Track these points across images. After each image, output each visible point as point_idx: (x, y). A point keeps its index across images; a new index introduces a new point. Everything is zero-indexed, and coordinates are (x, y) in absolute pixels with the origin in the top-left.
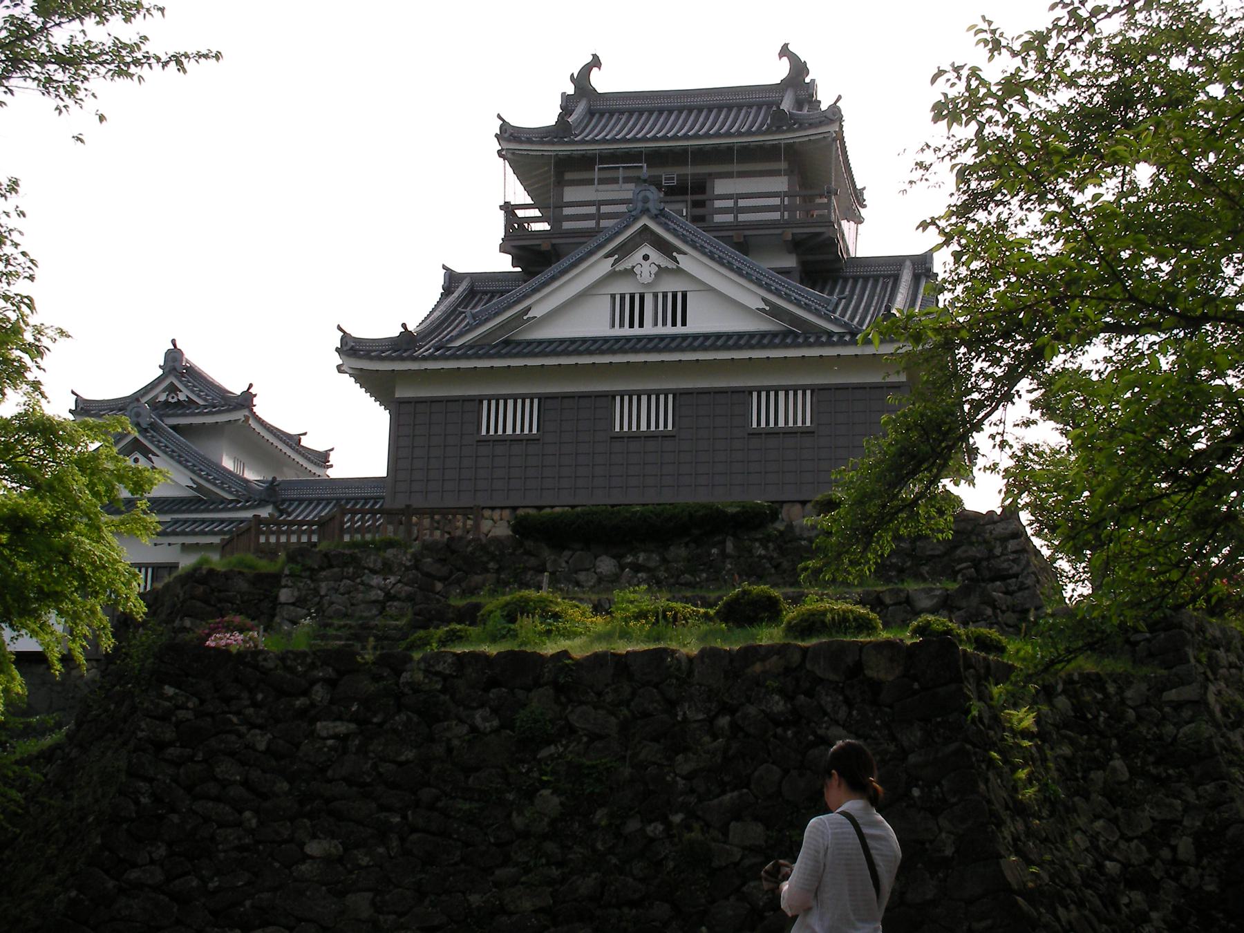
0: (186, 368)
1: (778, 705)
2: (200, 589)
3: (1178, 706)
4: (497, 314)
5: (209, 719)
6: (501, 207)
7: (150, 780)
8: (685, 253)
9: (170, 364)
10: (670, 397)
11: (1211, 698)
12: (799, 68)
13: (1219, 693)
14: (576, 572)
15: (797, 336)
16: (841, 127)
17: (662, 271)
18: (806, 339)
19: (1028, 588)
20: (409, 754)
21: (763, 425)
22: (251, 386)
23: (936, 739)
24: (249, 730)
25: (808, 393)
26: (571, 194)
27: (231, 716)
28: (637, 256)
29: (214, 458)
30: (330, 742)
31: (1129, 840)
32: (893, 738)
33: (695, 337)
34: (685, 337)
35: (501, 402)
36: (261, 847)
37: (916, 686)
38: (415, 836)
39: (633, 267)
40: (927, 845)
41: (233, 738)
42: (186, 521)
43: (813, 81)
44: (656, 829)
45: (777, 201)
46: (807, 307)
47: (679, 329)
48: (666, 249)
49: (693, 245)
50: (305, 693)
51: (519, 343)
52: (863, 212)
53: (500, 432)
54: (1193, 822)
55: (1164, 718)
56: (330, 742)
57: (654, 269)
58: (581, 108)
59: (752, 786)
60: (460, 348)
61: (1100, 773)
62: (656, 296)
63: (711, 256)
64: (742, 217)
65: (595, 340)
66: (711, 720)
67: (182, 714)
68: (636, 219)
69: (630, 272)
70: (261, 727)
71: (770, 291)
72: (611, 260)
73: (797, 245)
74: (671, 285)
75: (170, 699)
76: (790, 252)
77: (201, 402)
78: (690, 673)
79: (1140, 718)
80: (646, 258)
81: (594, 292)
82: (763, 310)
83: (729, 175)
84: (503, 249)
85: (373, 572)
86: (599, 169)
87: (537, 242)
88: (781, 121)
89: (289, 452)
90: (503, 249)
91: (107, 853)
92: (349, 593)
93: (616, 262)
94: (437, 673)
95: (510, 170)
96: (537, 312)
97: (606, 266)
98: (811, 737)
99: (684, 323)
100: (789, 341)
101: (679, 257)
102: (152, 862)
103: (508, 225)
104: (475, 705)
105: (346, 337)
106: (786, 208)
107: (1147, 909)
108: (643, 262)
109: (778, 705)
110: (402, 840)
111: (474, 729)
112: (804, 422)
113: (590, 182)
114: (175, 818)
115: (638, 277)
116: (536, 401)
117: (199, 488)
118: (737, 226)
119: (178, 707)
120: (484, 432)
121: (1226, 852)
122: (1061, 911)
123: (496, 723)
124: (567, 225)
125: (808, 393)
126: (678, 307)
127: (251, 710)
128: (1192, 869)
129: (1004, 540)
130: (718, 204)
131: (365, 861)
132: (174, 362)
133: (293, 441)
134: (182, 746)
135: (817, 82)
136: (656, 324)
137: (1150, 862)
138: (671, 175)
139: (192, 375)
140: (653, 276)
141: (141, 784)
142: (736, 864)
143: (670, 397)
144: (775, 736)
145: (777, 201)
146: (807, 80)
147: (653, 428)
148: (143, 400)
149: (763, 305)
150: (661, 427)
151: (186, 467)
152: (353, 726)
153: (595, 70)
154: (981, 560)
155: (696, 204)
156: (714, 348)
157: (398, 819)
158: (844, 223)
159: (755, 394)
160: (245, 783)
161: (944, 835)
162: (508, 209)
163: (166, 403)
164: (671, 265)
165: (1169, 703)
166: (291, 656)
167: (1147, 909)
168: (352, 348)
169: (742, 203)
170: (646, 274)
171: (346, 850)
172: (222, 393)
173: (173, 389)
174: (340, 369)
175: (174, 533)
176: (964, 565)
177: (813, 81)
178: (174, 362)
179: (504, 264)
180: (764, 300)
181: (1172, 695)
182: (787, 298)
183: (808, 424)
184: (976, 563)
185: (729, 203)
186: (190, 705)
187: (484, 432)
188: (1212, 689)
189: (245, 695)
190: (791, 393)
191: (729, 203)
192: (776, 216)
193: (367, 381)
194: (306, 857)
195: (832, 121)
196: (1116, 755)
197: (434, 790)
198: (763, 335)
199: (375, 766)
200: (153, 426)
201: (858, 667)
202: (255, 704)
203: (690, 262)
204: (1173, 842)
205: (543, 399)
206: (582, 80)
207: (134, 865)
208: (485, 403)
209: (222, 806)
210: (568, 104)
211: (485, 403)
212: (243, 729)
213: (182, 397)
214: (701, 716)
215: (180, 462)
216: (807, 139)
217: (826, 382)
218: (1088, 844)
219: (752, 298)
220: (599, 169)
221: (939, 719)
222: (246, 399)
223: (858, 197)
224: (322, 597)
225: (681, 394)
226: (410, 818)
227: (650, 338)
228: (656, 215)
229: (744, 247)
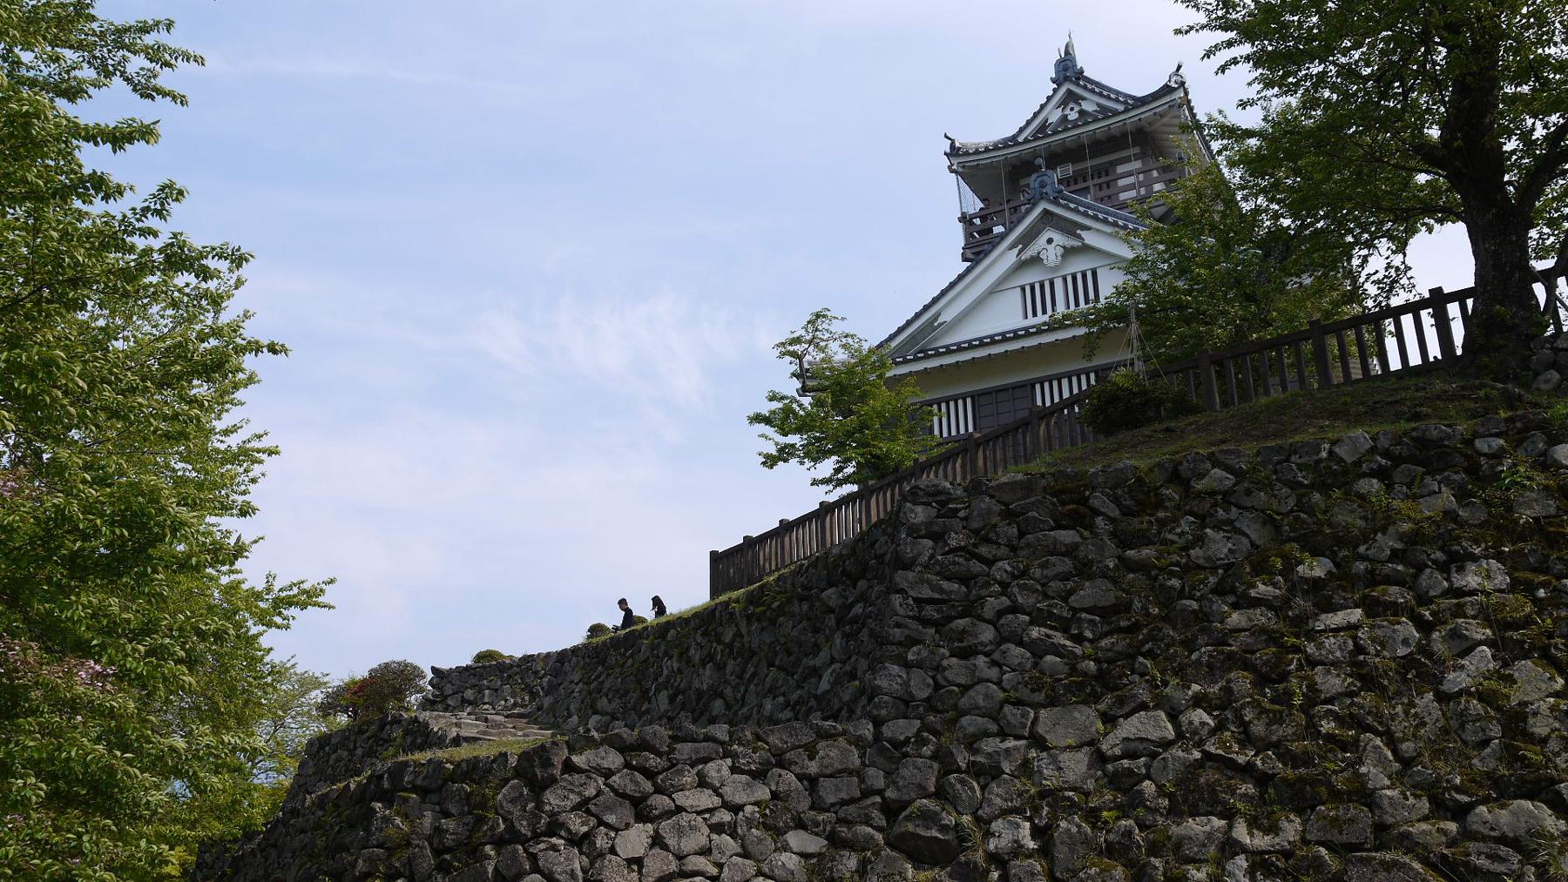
8: (1089, 229)
10: (969, 401)
17: (1068, 252)
28: (1042, 240)
35: (1055, 383)
39: (1039, 253)
48: (1070, 228)
57: (1060, 251)
68: (1034, 205)
69: (1036, 260)
72: (1016, 251)
80: (1050, 241)
93: (1020, 252)
96: (947, 317)
97: (1011, 258)
101: (1084, 234)
106: (1141, 185)
108: (1048, 247)
132: (1068, 71)
140: (1059, 258)
143: (969, 401)
164: (1076, 243)
170: (1052, 258)
205: (975, 396)
216: (1152, 113)
217: (1108, 361)
225: (979, 395)
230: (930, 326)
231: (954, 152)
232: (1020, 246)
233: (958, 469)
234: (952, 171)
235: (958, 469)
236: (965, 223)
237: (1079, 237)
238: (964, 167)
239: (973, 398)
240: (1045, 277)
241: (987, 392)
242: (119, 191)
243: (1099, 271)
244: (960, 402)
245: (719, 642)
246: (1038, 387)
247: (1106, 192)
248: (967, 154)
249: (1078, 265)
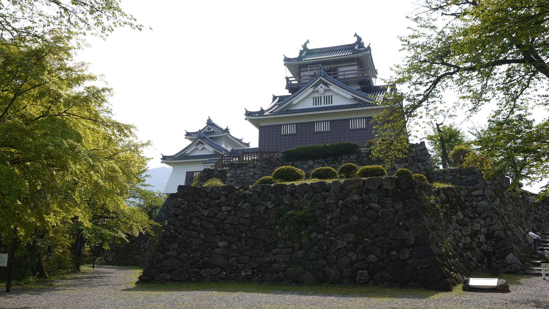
0: (212, 123)
1: (357, 198)
2: (206, 174)
3: (477, 196)
4: (284, 104)
5: (191, 207)
6: (285, 78)
7: (174, 225)
9: (208, 123)
11: (486, 194)
12: (359, 39)
13: (488, 192)
14: (302, 165)
15: (361, 105)
16: (371, 51)
17: (325, 90)
18: (363, 105)
19: (429, 164)
20: (247, 215)
22: (228, 127)
23: (407, 207)
24: (203, 210)
26: (302, 74)
27: (197, 206)
28: (319, 87)
29: (219, 145)
30: (225, 213)
31: (465, 236)
32: (393, 207)
33: (335, 106)
34: (332, 107)
36: (205, 244)
37: (399, 190)
38: (250, 240)
40: (406, 241)
41: (197, 212)
42: (212, 160)
43: (363, 42)
44: (320, 236)
45: (354, 72)
46: (363, 97)
47: (330, 105)
49: (333, 83)
50: (219, 199)
51: (290, 111)
52: (377, 76)
53: (355, 128)
54: (484, 230)
55: (473, 200)
56: (225, 213)
57: (324, 90)
58: (305, 53)
59: (350, 223)
60: (275, 113)
61: (455, 216)
62: (324, 97)
63: (338, 86)
64: (346, 77)
65: (309, 109)
66: (336, 203)
67: (183, 206)
69: (317, 91)
70: (206, 209)
71: (353, 93)
72: (313, 88)
73: (360, 83)
74: (328, 94)
75: (180, 202)
76: (359, 85)
77: (216, 131)
78: (330, 188)
79: (466, 201)
80: (321, 87)
81: (309, 97)
82: (352, 99)
83: (342, 67)
84: (286, 88)
85: (251, 168)
86: (309, 67)
87: (295, 86)
88: (355, 52)
89: (239, 143)
90: (286, 88)
91: (161, 247)
92: (245, 173)
93: (314, 89)
94: (256, 191)
95: (287, 69)
96: (294, 103)
98: (367, 207)
99: (332, 103)
100: (359, 106)
101: (330, 86)
102: (174, 249)
103: (287, 82)
104: (267, 200)
105: (247, 111)
107: (472, 257)
109: (357, 198)
110: (246, 241)
111: (267, 207)
112: (364, 127)
113: (307, 71)
114: (181, 236)
116: (295, 125)
117: (215, 152)
118: (345, 79)
119: (182, 204)
120: (282, 133)
121: (495, 239)
122: (449, 260)
123: (273, 205)
124: (302, 82)
125: (364, 119)
126: (329, 99)
127: (203, 204)
128: (484, 244)
129: (421, 151)
130: (340, 74)
131: (235, 248)
132: (210, 123)
133: (240, 141)
134: (183, 215)
135: (364, 42)
136: (325, 104)
137: (471, 243)
138: (327, 67)
139: (214, 125)
141: (171, 226)
142: (345, 247)
144: (356, 207)
145: (354, 72)
146: (362, 42)
147: (325, 130)
148: (202, 132)
149: (352, 97)
150: (327, 130)
151: (212, 147)
152: (232, 208)
153: (308, 44)
154: (415, 157)
155: (334, 74)
156: (339, 109)
157: (245, 235)
158: (373, 78)
159: (351, 120)
160: (201, 225)
161: (411, 237)
162: (287, 78)
163: (208, 132)
165: (474, 195)
166: (215, 188)
167: (472, 257)
168: (248, 114)
169: (346, 73)
170: (321, 91)
171: (229, 244)
172: (221, 129)
173: (209, 129)
174: (246, 119)
175: (209, 163)
176: (410, 158)
177: (363, 42)
178: (210, 123)
179: (287, 93)
180: (352, 96)
181: (476, 193)
182: (358, 95)
183: (365, 127)
184: (413, 158)
185: (343, 73)
186: (186, 203)
187: (282, 133)
188: (486, 191)
189: (202, 200)
191: (343, 73)
192: (355, 75)
193: (252, 121)
194: (218, 247)
195: (368, 50)
196: (459, 211)
197: (255, 226)
198: (352, 105)
199: (238, 219)
200: (204, 137)
201: (381, 185)
202: (204, 202)
203: (333, 88)
204: (478, 236)
205: (297, 124)
206: (305, 46)
207: (169, 250)
208: (316, 123)
209: (194, 232)
210: (301, 52)
211: (316, 123)
212: (201, 209)
213: (212, 130)
214: (333, 201)
215: (210, 146)
218: (453, 238)
219: (349, 96)
220: (309, 67)
221: (407, 201)
222: (227, 130)
223: (376, 72)
224: (238, 175)
226: (248, 234)
227: (323, 108)
228: (324, 76)
229: (347, 84)
233: (546, 248)
235: (546, 248)
237: (329, 87)
239: (365, 118)
240: (319, 96)
242: (406, 100)
243: (333, 96)
245: (369, 266)
247: (335, 76)
249: (328, 94)
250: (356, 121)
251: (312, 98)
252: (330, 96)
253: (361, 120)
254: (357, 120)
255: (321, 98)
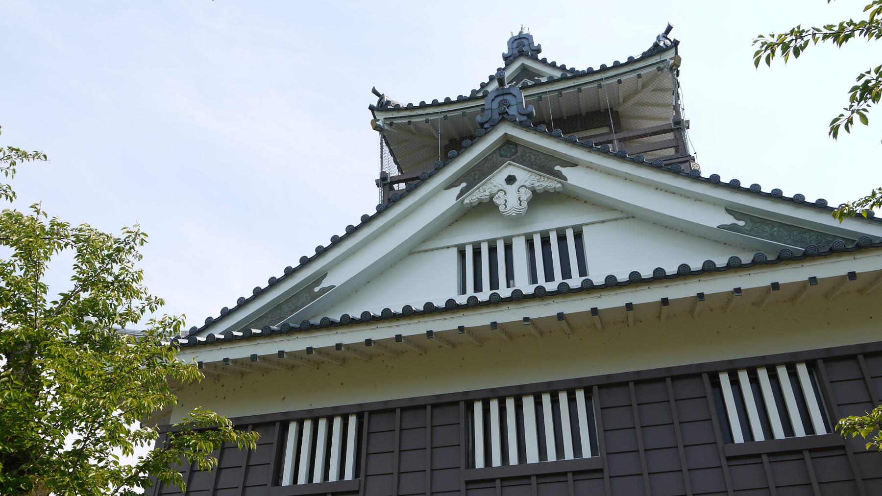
10: (352, 421)
21: (569, 454)
25: (580, 396)
28: (498, 179)
53: (513, 460)
57: (526, 195)
72: (457, 190)
80: (511, 180)
82: (732, 227)
97: (449, 200)
101: (566, 171)
108: (508, 188)
115: (501, 208)
120: (480, 463)
140: (525, 204)
143: (352, 421)
164: (552, 184)
180: (731, 210)
183: (587, 453)
187: (480, 463)
190: (546, 400)
208: (478, 408)
211: (478, 408)
225: (371, 413)
230: (307, 290)
231: (382, 106)
232: (464, 185)
234: (376, 128)
236: (384, 186)
237: (559, 175)
238: (391, 124)
239: (360, 417)
241: (385, 410)
243: (587, 233)
244: (307, 426)
246: (293, 428)
248: (397, 108)
250: (519, 408)
251: (454, 252)
252: (570, 236)
253: (555, 402)
254: (528, 403)
255: (508, 248)
